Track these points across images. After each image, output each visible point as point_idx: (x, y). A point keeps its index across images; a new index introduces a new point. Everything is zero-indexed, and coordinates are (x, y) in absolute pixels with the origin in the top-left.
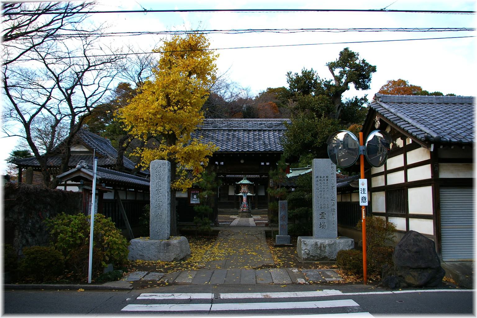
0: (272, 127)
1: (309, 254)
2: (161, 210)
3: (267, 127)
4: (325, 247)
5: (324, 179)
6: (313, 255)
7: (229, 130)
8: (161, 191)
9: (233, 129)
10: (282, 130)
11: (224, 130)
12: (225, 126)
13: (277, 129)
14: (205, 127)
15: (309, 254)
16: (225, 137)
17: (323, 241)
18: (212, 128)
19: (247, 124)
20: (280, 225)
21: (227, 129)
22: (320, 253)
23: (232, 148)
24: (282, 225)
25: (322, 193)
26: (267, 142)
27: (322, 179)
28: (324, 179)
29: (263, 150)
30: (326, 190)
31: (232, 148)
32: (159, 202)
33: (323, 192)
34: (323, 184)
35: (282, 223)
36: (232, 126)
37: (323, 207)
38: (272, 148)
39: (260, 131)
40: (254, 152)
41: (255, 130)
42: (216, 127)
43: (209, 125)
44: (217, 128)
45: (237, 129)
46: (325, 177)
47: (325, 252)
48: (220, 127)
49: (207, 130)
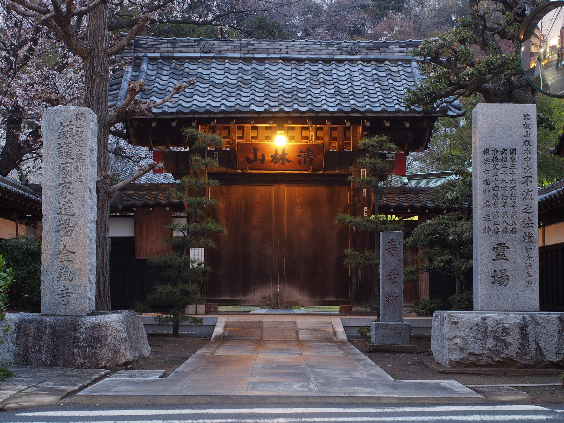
0: (359, 51)
1: (466, 349)
2: (73, 236)
3: (347, 51)
4: (505, 331)
5: (504, 156)
6: (476, 352)
7: (244, 59)
8: (71, 187)
9: (257, 55)
10: (386, 60)
11: (230, 59)
12: (234, 50)
13: (372, 57)
14: (181, 52)
15: (466, 349)
16: (235, 77)
17: (502, 316)
18: (198, 55)
19: (293, 45)
20: (383, 293)
21: (238, 55)
22: (496, 345)
23: (253, 101)
24: (388, 297)
25: (500, 193)
26: (345, 88)
27: (499, 157)
28: (504, 156)
29: (336, 109)
30: (509, 186)
31: (253, 101)
32: (66, 217)
33: (500, 189)
34: (501, 171)
35: (387, 290)
36: (254, 50)
37: (501, 229)
38: (359, 105)
39: (327, 61)
40: (313, 115)
41: (314, 61)
42: (210, 52)
43: (192, 46)
44: (212, 55)
45: (265, 56)
46: (508, 152)
47: (507, 345)
48: (220, 52)
49: (187, 58)
